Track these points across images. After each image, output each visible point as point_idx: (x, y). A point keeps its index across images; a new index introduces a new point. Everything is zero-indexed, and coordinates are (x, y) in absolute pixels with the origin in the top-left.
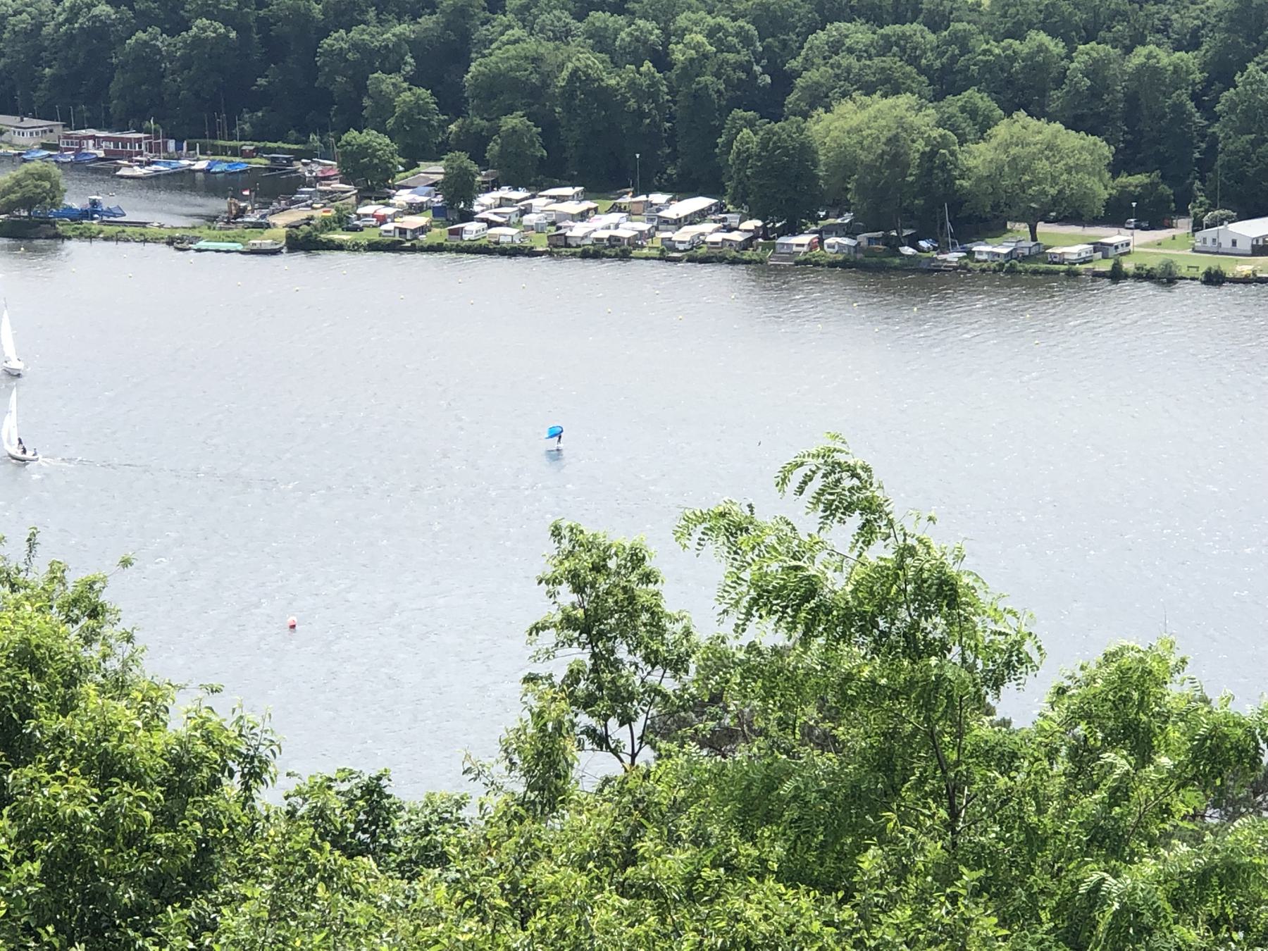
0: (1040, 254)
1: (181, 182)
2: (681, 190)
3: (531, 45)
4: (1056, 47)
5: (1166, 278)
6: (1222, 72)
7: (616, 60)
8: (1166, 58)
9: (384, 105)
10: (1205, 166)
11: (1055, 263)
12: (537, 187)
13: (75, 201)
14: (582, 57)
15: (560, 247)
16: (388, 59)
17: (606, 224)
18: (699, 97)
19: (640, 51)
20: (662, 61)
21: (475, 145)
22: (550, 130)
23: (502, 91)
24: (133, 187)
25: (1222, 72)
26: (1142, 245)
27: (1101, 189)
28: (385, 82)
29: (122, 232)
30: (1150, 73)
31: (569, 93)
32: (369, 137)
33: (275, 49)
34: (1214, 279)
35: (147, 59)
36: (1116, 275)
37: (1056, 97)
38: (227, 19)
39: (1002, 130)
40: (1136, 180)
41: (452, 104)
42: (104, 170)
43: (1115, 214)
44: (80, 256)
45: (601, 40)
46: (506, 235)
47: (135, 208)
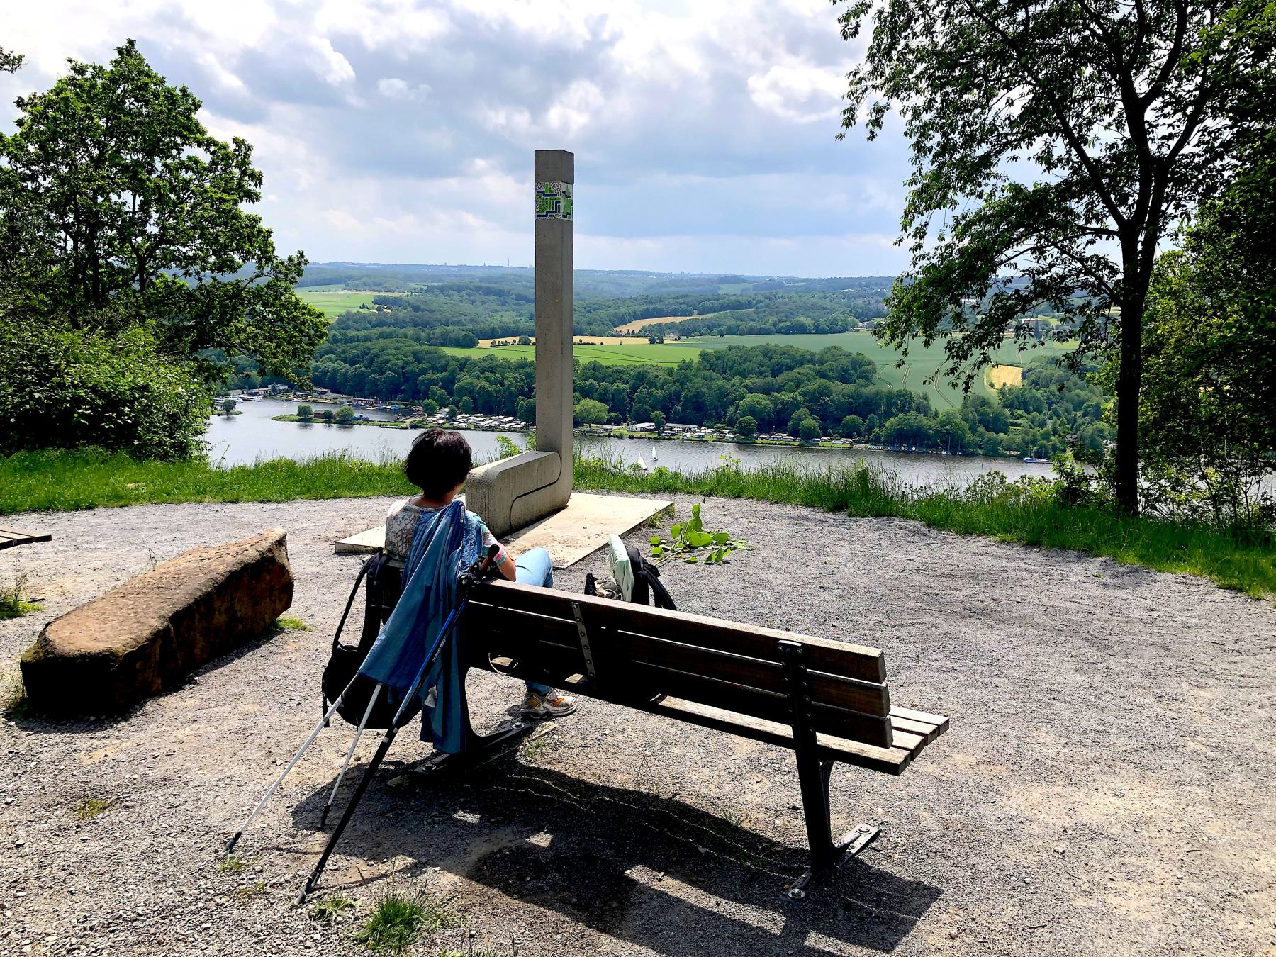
0: (592, 431)
1: (384, 410)
2: (507, 415)
3: (470, 380)
4: (595, 383)
5: (621, 437)
6: (634, 390)
7: (491, 385)
8: (622, 386)
9: (434, 394)
10: (630, 411)
11: (802, 330)
12: (471, 414)
13: (357, 415)
14: (483, 383)
15: (477, 428)
16: (435, 382)
17: (487, 423)
18: (511, 393)
19: (496, 382)
20: (502, 384)
21: (457, 405)
22: (475, 400)
23: (463, 391)
24: (620, 301)
25: (634, 390)
26: (615, 429)
27: (605, 416)
28: (434, 388)
29: (367, 423)
30: (617, 391)
31: (479, 392)
32: (430, 401)
33: (406, 380)
34: (632, 437)
35: (375, 382)
36: (609, 436)
37: (596, 395)
38: (395, 372)
39: (582, 402)
40: (613, 414)
41: (451, 394)
42: (363, 408)
43: (609, 422)
44: (357, 429)
45: (487, 379)
46: (463, 425)
47: (372, 417)
